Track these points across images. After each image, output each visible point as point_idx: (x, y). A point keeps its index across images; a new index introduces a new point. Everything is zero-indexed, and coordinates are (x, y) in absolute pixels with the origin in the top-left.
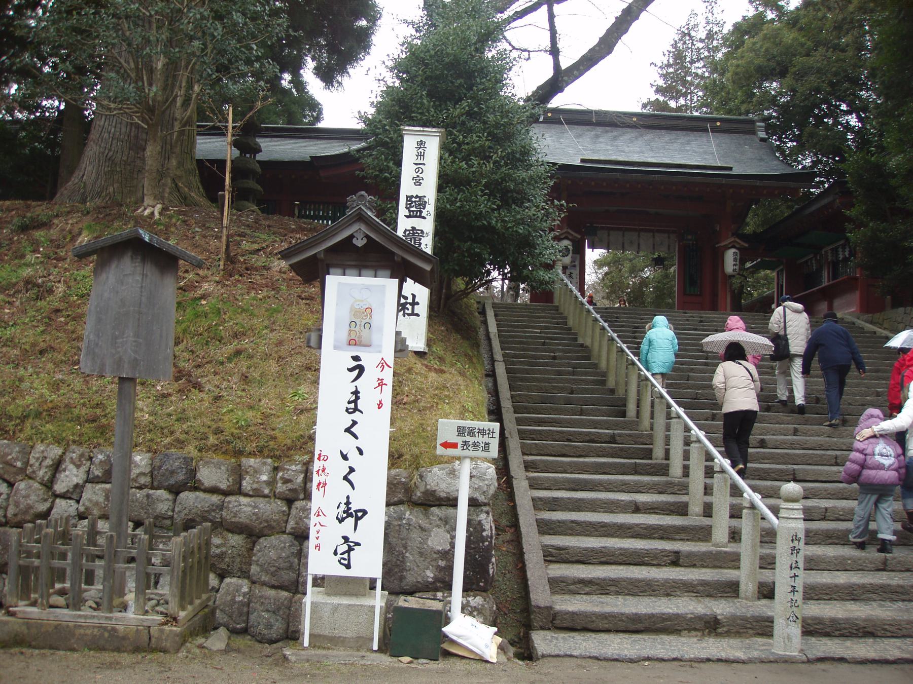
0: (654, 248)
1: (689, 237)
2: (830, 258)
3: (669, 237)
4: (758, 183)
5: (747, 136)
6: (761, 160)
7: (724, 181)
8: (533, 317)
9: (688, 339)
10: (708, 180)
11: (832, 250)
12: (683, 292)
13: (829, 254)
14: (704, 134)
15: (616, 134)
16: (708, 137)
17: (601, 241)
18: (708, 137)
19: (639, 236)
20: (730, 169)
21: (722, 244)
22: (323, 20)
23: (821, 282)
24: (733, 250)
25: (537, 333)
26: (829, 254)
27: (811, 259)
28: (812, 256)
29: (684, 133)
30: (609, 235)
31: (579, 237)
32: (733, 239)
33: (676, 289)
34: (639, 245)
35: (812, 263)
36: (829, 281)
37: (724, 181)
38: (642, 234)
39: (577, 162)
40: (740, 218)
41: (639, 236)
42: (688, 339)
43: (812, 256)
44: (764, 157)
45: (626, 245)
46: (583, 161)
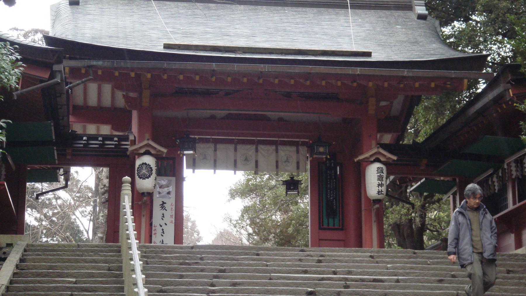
0: (277, 167)
1: (321, 149)
2: (514, 173)
3: (298, 152)
4: (406, 73)
5: (400, 13)
6: (416, 42)
7: (358, 71)
8: (77, 261)
9: (287, 285)
10: (338, 70)
11: (516, 161)
12: (321, 225)
13: (513, 169)
14: (342, 11)
15: (220, 12)
16: (347, 15)
17: (205, 158)
18: (347, 15)
19: (257, 150)
20: (369, 54)
21: (361, 157)
22: (513, 104)
23: (506, 207)
24: (377, 165)
25: (71, 282)
26: (513, 169)
27: (491, 175)
28: (490, 172)
29: (315, 10)
30: (215, 150)
31: (185, 157)
32: (375, 150)
33: (309, 224)
34: (257, 162)
35: (493, 182)
36: (514, 203)
37: (358, 71)
38: (261, 147)
39: (160, 49)
40: (397, 123)
41: (257, 150)
42: (287, 285)
43: (490, 172)
44: (420, 39)
45: (239, 163)
46: (167, 46)
